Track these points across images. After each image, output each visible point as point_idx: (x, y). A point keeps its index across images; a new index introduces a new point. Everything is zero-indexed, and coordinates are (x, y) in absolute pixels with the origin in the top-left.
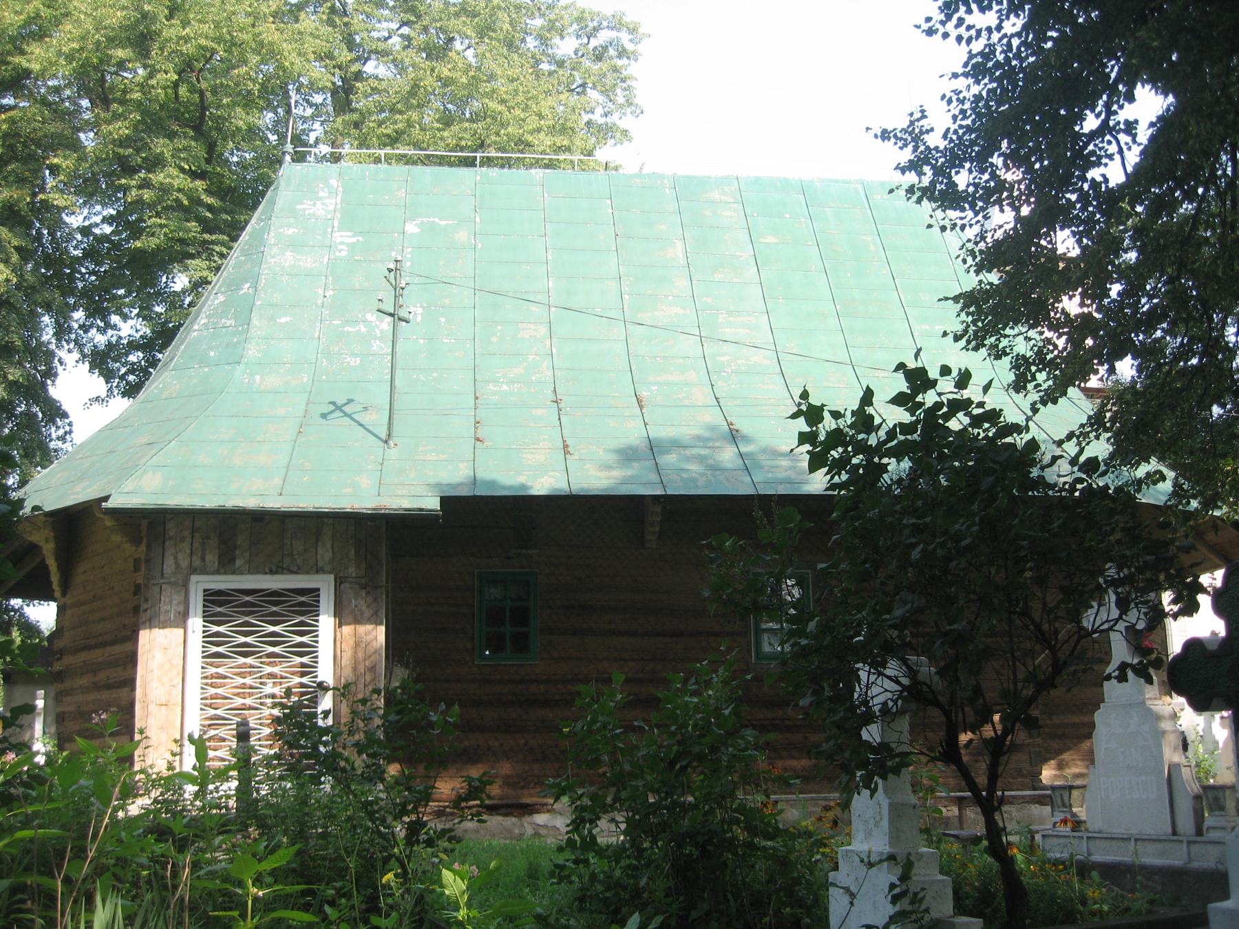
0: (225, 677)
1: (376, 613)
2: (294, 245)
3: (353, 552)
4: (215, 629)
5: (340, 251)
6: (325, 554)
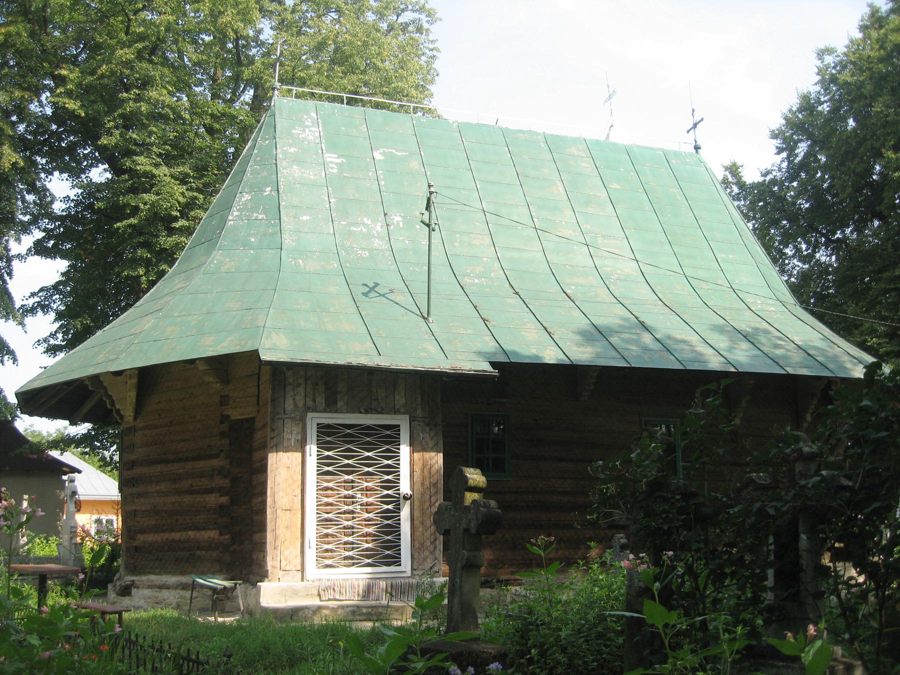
1: (437, 444)
2: (297, 160)
3: (419, 399)
4: (327, 453)
5: (332, 168)
6: (400, 400)
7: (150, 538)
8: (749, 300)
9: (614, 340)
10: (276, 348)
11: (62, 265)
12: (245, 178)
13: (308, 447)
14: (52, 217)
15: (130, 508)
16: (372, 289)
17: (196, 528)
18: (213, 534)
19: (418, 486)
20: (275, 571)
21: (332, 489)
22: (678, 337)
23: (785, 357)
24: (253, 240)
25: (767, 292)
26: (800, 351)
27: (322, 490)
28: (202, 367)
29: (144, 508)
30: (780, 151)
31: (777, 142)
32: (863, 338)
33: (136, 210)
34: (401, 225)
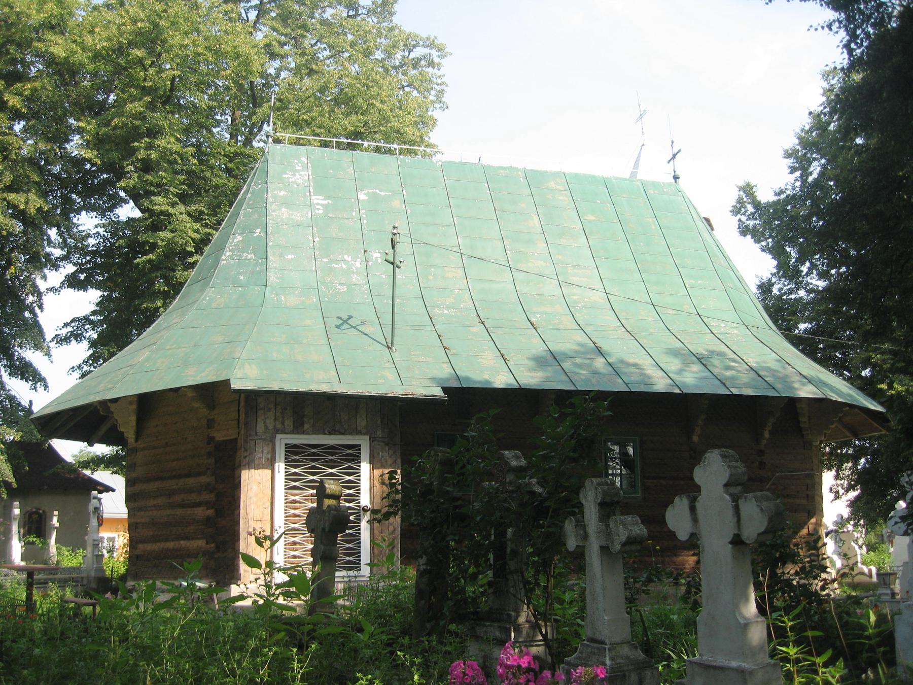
0: (300, 502)
1: (395, 462)
2: (287, 203)
3: (379, 421)
5: (318, 209)
7: (149, 547)
8: (712, 323)
9: (567, 365)
10: (246, 377)
11: (94, 295)
12: (238, 221)
13: (277, 465)
14: (84, 251)
15: (133, 520)
16: (345, 322)
17: (187, 538)
18: (201, 543)
19: (377, 500)
20: (247, 574)
21: (300, 502)
22: (631, 360)
23: (733, 378)
24: (242, 278)
25: (733, 316)
26: (752, 372)
27: (291, 502)
28: (190, 394)
29: (143, 520)
30: (793, 170)
31: (790, 162)
32: (867, 354)
33: (154, 246)
34: (379, 261)
